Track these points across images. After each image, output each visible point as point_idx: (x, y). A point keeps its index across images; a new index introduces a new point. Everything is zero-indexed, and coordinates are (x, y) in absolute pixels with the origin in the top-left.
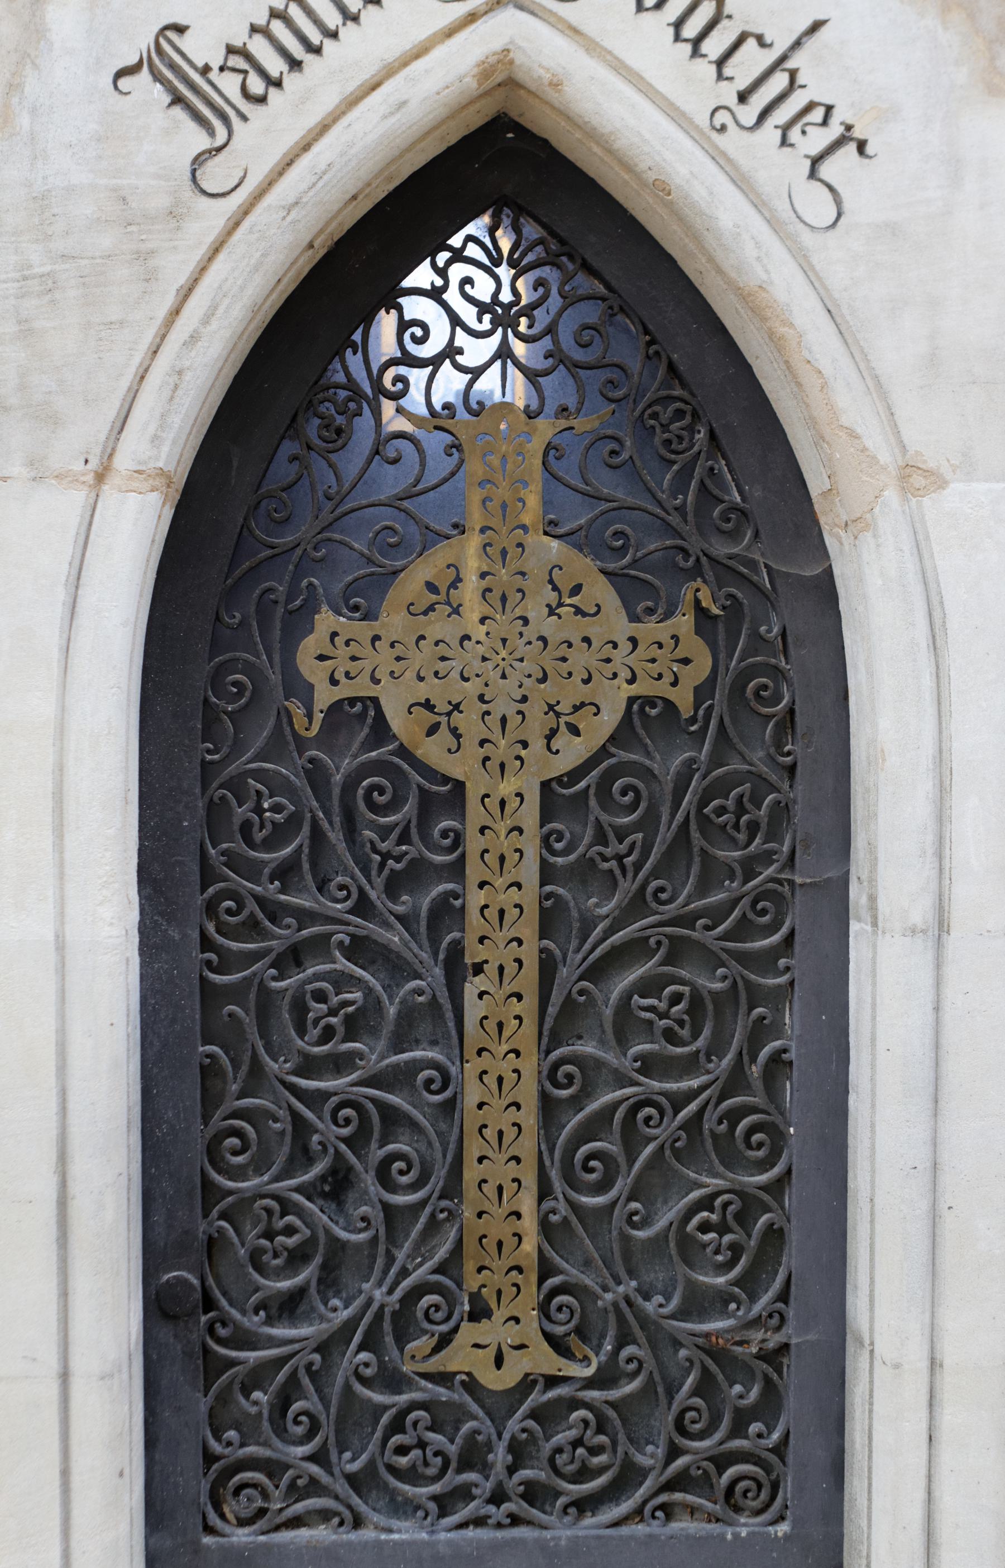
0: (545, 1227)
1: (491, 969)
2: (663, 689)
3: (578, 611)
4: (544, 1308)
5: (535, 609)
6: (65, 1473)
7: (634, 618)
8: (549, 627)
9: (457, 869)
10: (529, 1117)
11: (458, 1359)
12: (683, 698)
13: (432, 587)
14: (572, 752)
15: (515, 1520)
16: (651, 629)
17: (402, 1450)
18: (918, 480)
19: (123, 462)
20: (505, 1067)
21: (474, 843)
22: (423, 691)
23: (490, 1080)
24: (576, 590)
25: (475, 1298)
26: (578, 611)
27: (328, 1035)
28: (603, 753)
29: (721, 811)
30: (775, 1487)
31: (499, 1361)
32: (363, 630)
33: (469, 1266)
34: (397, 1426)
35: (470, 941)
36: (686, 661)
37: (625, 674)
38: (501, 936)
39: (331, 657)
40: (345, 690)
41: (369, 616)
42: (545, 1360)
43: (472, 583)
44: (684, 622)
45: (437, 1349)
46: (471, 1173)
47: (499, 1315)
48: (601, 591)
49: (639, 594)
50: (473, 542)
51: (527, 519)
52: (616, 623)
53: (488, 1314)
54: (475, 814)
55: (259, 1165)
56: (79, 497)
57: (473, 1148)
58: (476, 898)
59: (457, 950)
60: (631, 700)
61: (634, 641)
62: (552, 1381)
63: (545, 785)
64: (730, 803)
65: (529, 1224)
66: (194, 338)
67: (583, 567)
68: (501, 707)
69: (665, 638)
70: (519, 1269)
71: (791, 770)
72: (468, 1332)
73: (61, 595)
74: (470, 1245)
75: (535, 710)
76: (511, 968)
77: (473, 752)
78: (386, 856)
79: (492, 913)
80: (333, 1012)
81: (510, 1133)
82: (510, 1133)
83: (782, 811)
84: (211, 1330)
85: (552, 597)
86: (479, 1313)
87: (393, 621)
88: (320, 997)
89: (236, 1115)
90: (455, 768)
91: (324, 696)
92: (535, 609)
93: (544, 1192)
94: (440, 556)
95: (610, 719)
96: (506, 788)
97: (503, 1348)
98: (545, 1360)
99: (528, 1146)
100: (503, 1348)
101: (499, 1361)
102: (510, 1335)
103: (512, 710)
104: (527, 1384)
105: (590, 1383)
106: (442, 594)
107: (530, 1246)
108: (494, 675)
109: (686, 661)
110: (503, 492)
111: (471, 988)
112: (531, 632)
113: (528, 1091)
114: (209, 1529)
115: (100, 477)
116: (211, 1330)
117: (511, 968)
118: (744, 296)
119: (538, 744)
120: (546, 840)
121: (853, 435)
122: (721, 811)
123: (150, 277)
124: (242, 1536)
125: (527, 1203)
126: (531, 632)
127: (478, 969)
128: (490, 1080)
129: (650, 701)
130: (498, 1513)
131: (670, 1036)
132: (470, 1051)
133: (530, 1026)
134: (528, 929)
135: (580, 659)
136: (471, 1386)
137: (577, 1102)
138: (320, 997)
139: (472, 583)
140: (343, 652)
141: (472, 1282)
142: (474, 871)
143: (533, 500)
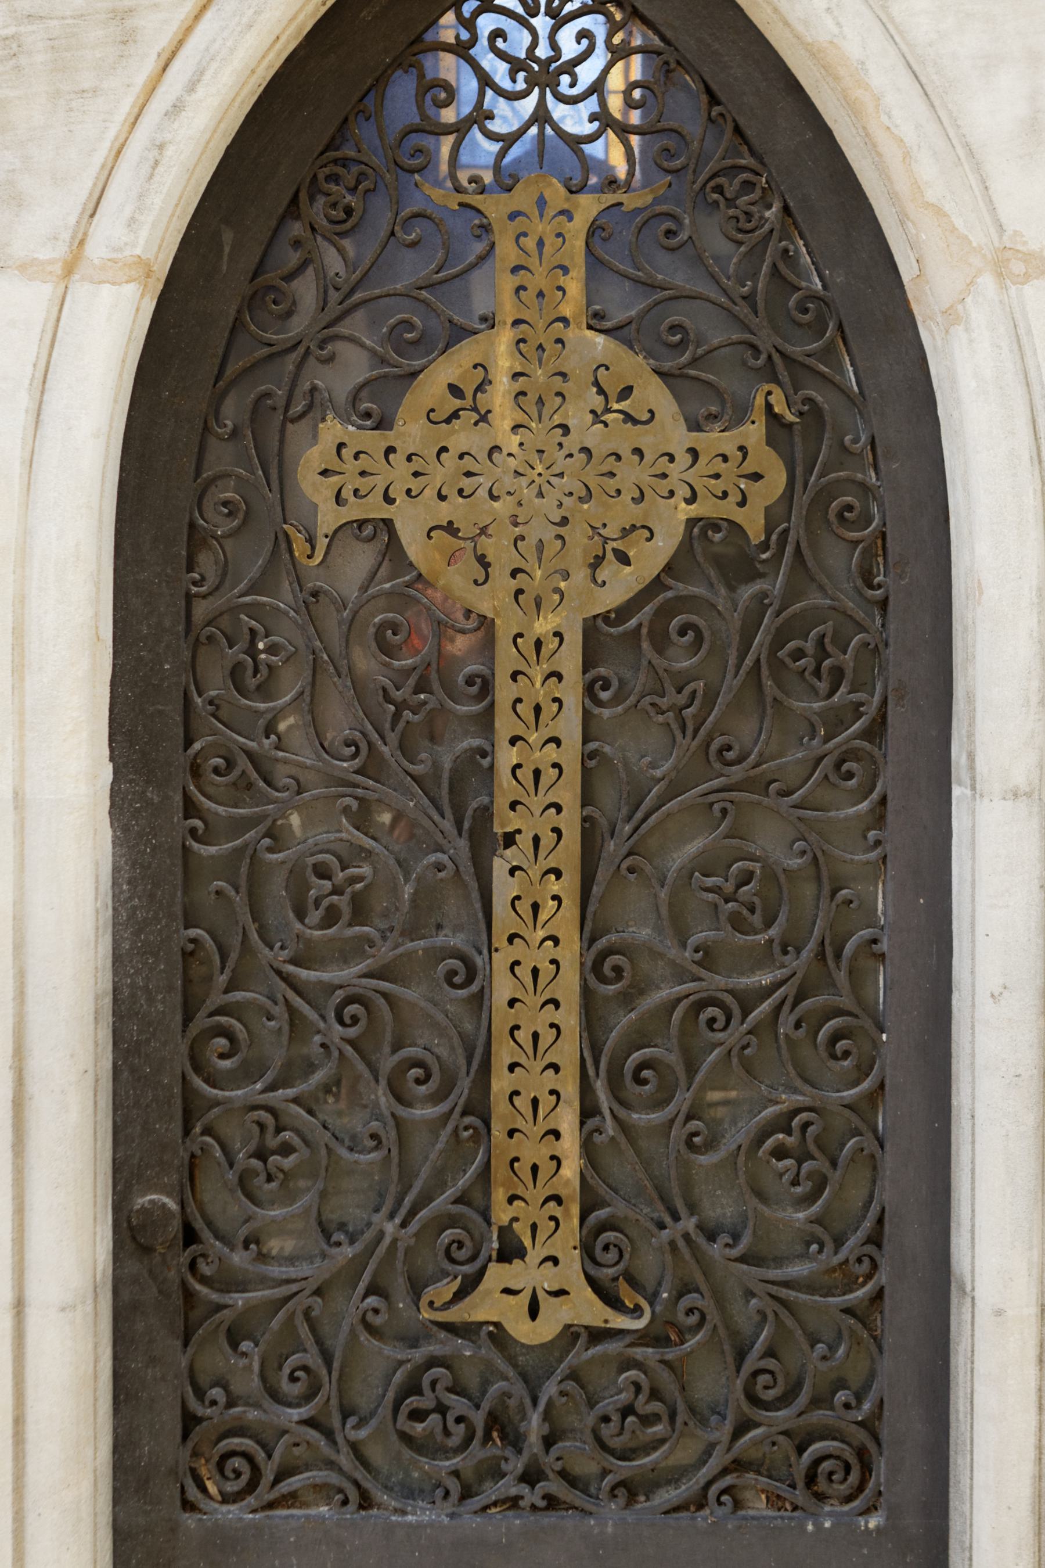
0: (588, 1147)
1: (524, 841)
2: (729, 509)
3: (629, 418)
4: (587, 1250)
5: (577, 416)
6: (19, 1421)
7: (695, 426)
8: (594, 436)
9: (486, 721)
10: (569, 1018)
11: (486, 1306)
12: (753, 522)
13: (455, 390)
14: (620, 585)
15: (552, 1503)
16: (717, 440)
17: (418, 1415)
18: (1018, 267)
19: (96, 250)
20: (541, 959)
21: (504, 692)
22: (444, 512)
23: (524, 972)
24: (626, 392)
25: (505, 1232)
26: (629, 418)
27: (331, 917)
28: (657, 585)
29: (799, 654)
30: (867, 1469)
31: (534, 1311)
32: (374, 441)
33: (499, 1195)
34: (412, 1387)
35: (501, 803)
36: (756, 477)
37: (684, 492)
38: (537, 803)
39: (327, 470)
40: (353, 511)
41: (383, 424)
42: (586, 1308)
43: (502, 386)
44: (754, 432)
45: (460, 1295)
46: (501, 1083)
47: (534, 1255)
48: (653, 394)
49: (707, 403)
50: (504, 338)
51: (567, 311)
52: (678, 437)
53: (520, 1253)
54: (506, 658)
55: (247, 1073)
56: (44, 291)
57: (503, 1053)
58: (507, 757)
59: (486, 814)
60: (691, 522)
61: (694, 453)
62: (598, 1335)
63: (591, 629)
64: (809, 646)
65: (570, 1145)
66: (177, 108)
67: (631, 365)
68: (539, 531)
69: (730, 448)
70: (558, 1199)
71: (884, 604)
72: (497, 1275)
73: (24, 400)
74: (500, 1171)
75: (578, 535)
76: (548, 839)
77: (502, 583)
78: (400, 707)
79: (526, 775)
80: (336, 891)
81: (547, 1036)
82: (547, 1036)
83: (874, 651)
84: (193, 1266)
85: (597, 402)
86: (510, 1251)
87: (411, 431)
88: (322, 872)
89: (220, 1011)
90: (485, 603)
91: (328, 518)
92: (577, 416)
93: (588, 1111)
94: (466, 353)
95: (664, 546)
96: (543, 626)
97: (538, 1295)
98: (586, 1308)
99: (568, 1051)
100: (538, 1295)
101: (534, 1311)
102: (547, 1279)
103: (549, 533)
104: (570, 1335)
105: (644, 1338)
106: (468, 401)
107: (570, 1171)
108: (528, 493)
109: (756, 477)
110: (538, 279)
111: (499, 867)
112: (572, 443)
113: (569, 986)
114: (188, 1506)
115: (70, 268)
116: (193, 1266)
117: (548, 839)
118: (814, 52)
119: (580, 575)
120: (589, 690)
121: (939, 212)
122: (799, 654)
123: (127, 39)
124: (232, 1512)
125: (567, 1120)
126: (572, 443)
127: (509, 840)
128: (524, 972)
129: (713, 525)
130: (532, 1496)
131: (737, 923)
132: (500, 940)
133: (571, 910)
134: (568, 793)
135: (631, 474)
136: (499, 1336)
137: (627, 999)
138: (322, 872)
139: (502, 386)
140: (351, 466)
141: (502, 1214)
142: (505, 725)
143: (575, 286)
